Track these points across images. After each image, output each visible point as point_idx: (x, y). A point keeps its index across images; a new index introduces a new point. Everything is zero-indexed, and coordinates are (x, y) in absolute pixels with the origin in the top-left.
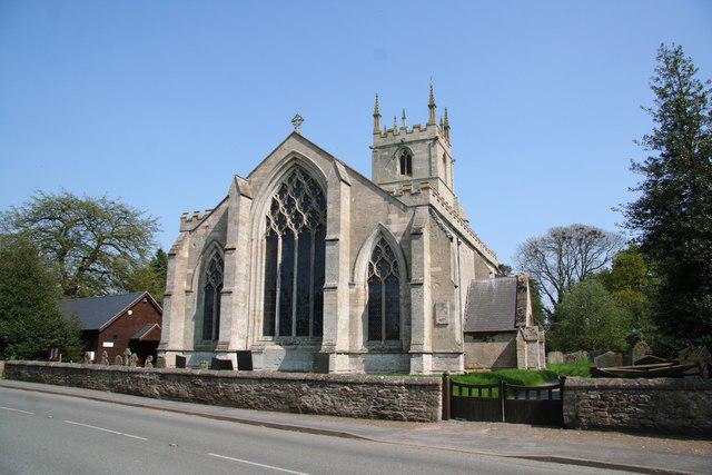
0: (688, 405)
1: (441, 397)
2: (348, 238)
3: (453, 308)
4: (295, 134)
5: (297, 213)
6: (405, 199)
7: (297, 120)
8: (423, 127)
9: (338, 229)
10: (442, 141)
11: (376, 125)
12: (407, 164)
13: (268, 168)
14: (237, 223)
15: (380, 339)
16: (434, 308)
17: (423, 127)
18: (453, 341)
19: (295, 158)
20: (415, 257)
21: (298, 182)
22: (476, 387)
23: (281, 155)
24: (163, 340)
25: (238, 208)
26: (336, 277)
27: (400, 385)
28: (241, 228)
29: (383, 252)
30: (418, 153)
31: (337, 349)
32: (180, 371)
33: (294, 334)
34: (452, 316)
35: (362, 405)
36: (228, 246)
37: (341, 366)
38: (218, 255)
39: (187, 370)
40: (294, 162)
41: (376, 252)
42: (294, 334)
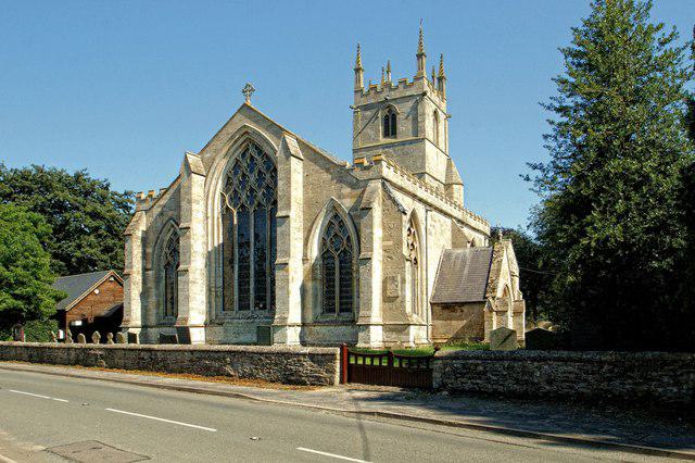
0: (533, 373)
1: (338, 366)
2: (301, 214)
3: (403, 281)
4: (245, 109)
5: (252, 190)
6: (357, 173)
7: (248, 90)
8: (409, 81)
9: (288, 206)
10: (434, 96)
11: (358, 81)
12: (390, 128)
13: (225, 137)
14: (190, 202)
15: (334, 311)
16: (384, 282)
17: (409, 81)
18: (404, 313)
19: (246, 132)
20: (364, 232)
21: (252, 158)
22: (406, 358)
23: (231, 130)
24: (125, 317)
25: (190, 187)
26: (287, 253)
27: (304, 355)
28: (194, 206)
29: (337, 227)
30: (402, 110)
31: (289, 321)
32: (132, 345)
33: (252, 309)
34: (403, 289)
35: (275, 372)
36: (182, 225)
37: (198, 338)
38: (175, 233)
39: (138, 345)
40: (246, 136)
41: (329, 228)
42: (252, 309)
